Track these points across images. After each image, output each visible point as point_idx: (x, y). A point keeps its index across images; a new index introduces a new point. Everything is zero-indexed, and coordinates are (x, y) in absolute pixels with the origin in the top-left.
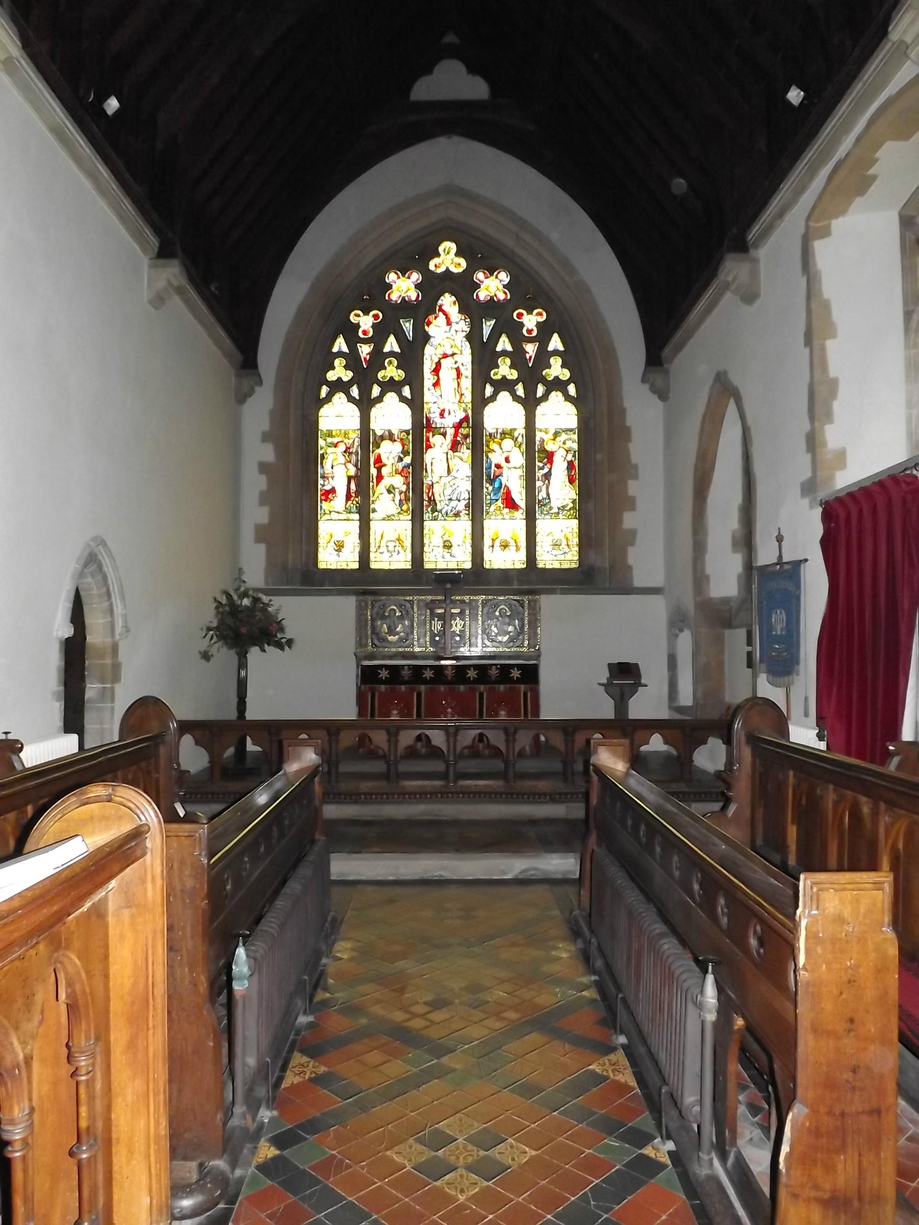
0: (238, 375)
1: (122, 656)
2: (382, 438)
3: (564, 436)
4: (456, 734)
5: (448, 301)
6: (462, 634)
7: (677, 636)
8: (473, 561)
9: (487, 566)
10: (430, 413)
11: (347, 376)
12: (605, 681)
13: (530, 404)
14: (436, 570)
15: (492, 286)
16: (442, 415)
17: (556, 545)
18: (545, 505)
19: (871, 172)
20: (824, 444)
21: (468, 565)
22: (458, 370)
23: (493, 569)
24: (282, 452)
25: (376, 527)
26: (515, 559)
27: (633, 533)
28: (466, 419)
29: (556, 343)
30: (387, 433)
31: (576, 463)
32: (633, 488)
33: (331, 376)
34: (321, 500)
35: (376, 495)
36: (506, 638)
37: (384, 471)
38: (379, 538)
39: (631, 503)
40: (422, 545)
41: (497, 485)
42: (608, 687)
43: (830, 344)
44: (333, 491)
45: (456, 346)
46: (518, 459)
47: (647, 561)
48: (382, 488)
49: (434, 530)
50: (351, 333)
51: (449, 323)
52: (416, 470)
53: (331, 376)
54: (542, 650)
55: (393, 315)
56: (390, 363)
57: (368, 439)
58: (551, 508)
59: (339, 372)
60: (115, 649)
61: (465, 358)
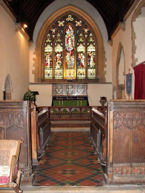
0: (29, 41)
1: (11, 95)
2: (57, 53)
3: (93, 53)
4: (71, 109)
6: (73, 91)
7: (114, 92)
11: (83, 41)
12: (100, 100)
13: (86, 47)
15: (78, 24)
16: (69, 49)
17: (91, 74)
19: (141, 11)
20: (134, 57)
24: (38, 56)
27: (106, 72)
29: (91, 35)
32: (106, 63)
33: (47, 41)
36: (81, 92)
37: (57, 60)
39: (105, 66)
42: (100, 102)
43: (135, 40)
44: (47, 64)
47: (109, 77)
51: (70, 31)
53: (47, 41)
54: (88, 95)
60: (10, 93)
61: (73, 38)
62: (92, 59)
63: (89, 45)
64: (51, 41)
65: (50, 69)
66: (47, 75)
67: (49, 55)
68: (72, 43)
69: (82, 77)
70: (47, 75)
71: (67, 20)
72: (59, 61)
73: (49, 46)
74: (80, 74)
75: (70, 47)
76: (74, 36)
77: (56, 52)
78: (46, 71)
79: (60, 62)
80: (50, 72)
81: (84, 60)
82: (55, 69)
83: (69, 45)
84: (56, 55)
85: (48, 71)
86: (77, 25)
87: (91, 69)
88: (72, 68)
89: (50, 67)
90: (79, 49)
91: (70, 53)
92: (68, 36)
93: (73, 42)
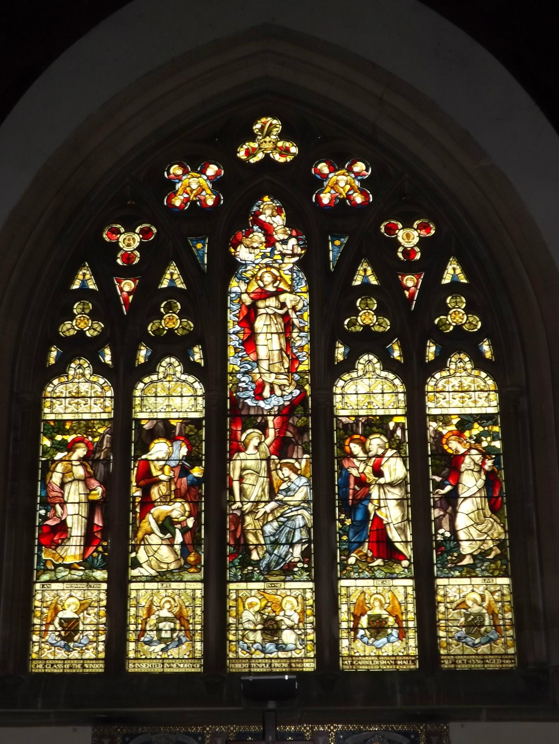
2: (154, 434)
3: (477, 429)
5: (269, 212)
8: (318, 657)
9: (345, 665)
10: (237, 390)
11: (92, 329)
13: (415, 376)
14: (250, 673)
15: (342, 184)
16: (259, 395)
17: (473, 624)
18: (449, 552)
21: (309, 666)
22: (286, 317)
23: (356, 673)
25: (139, 592)
26: (396, 650)
28: (301, 400)
29: (452, 272)
30: (160, 425)
31: (502, 475)
33: (68, 329)
34: (40, 546)
35: (140, 535)
37: (155, 493)
38: (143, 613)
40: (224, 627)
41: (359, 516)
44: (62, 528)
45: (282, 279)
46: (395, 468)
48: (150, 522)
49: (248, 599)
50: (105, 261)
51: (270, 242)
52: (211, 492)
53: (68, 329)
55: (176, 232)
56: (169, 308)
57: (127, 434)
58: (462, 557)
59: (82, 323)
61: (298, 299)
62: (471, 482)
63: (440, 364)
64: (99, 326)
65: (87, 580)
66: (51, 637)
67: (81, 452)
68: (288, 341)
69: (388, 650)
70: (51, 637)
71: (242, 154)
72: (166, 500)
73: (81, 368)
74: (364, 622)
75: (270, 378)
76: (308, 282)
77: (147, 426)
78: (49, 596)
79: (178, 510)
80: (84, 606)
81: (397, 493)
82: (136, 579)
83: (257, 361)
84: (146, 450)
85: (64, 595)
86: (326, 199)
87: (469, 572)
88: (288, 571)
89: (87, 563)
90: (352, 400)
91: (271, 433)
92: (254, 287)
93: (301, 340)
